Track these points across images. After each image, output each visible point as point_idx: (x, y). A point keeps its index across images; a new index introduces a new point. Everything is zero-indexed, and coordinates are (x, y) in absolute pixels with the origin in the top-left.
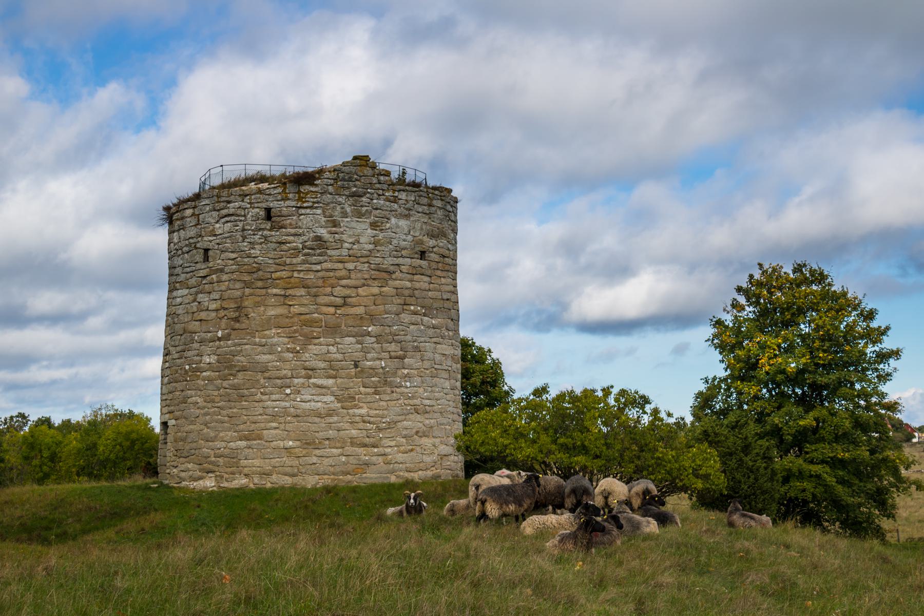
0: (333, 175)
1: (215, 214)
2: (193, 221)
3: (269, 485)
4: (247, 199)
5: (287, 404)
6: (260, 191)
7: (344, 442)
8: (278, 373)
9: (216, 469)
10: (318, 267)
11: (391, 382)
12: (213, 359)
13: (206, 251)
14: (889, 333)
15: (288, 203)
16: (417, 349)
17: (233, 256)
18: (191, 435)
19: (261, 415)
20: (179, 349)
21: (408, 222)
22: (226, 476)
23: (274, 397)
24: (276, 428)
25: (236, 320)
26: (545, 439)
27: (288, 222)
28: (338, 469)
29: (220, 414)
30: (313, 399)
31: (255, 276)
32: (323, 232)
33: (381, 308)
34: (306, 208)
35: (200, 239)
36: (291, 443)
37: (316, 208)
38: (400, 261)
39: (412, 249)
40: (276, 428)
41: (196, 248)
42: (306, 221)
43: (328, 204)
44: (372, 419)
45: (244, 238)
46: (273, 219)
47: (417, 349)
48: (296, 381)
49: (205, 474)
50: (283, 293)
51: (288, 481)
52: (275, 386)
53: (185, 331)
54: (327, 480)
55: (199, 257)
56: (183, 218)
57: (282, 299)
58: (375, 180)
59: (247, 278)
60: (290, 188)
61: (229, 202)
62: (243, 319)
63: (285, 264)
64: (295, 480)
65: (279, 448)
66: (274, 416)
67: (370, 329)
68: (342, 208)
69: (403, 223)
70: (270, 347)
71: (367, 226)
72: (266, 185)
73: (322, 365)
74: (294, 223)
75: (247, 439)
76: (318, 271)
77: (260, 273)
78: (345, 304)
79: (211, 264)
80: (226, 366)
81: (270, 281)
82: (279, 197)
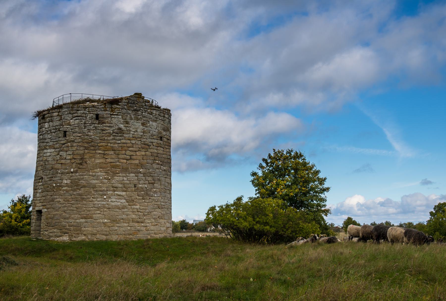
0: (127, 101)
1: (70, 115)
2: (58, 118)
3: (95, 239)
4: (87, 109)
5: (105, 203)
6: (93, 106)
7: (130, 221)
8: (100, 189)
9: (69, 232)
10: (119, 142)
11: (149, 194)
12: (69, 181)
13: (65, 132)
14: (326, 180)
15: (106, 112)
16: (159, 180)
17: (80, 135)
18: (57, 216)
19: (92, 207)
20: (50, 176)
21: (156, 124)
22: (74, 235)
23: (98, 199)
24: (99, 214)
25: (81, 164)
26: (250, 219)
27: (107, 121)
28: (126, 232)
29: (72, 207)
30: (116, 201)
31: (90, 144)
32: (122, 126)
33: (145, 161)
34: (115, 115)
35: (62, 126)
36: (106, 220)
37: (119, 115)
38: (153, 140)
39: (158, 136)
40: (99, 214)
41: (59, 130)
42: (114, 121)
43: (124, 114)
44: (141, 211)
45: (85, 127)
46: (100, 119)
47: (159, 180)
48: (109, 192)
49: (63, 234)
50: (103, 152)
51: (104, 238)
52: (99, 195)
53: (52, 168)
54: (122, 238)
55: (61, 135)
56: (51, 117)
57: (103, 155)
58: (144, 104)
59: (86, 145)
60: (108, 106)
61: (78, 110)
62: (84, 164)
63: (104, 140)
64: (108, 237)
65: (100, 223)
66: (99, 208)
67: (141, 170)
68: (130, 116)
69: (154, 124)
70: (97, 177)
71: (140, 124)
72: (96, 104)
73: (120, 185)
74: (109, 121)
75: (85, 218)
76: (119, 143)
77: (93, 143)
78: (131, 159)
79: (67, 138)
80: (75, 185)
81: (97, 147)
82: (103, 109)
